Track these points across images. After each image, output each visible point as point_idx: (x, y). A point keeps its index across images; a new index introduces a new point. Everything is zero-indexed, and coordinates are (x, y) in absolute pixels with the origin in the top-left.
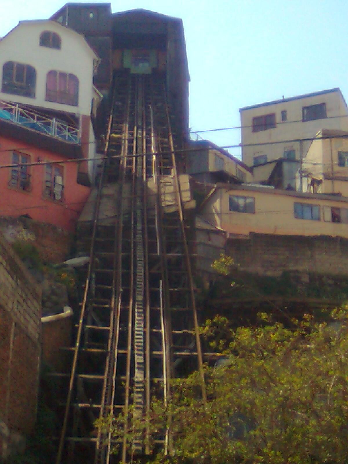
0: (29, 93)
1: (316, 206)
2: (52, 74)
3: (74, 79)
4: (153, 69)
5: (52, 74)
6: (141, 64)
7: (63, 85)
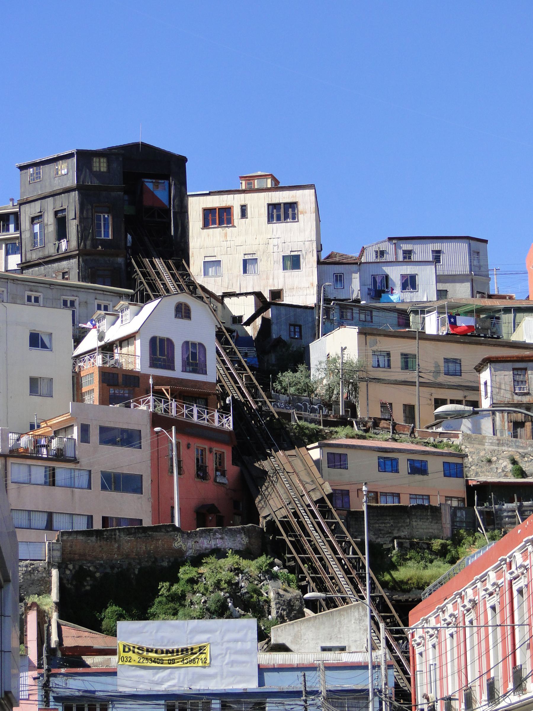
0: (171, 367)
1: (395, 459)
3: (201, 345)
5: (186, 344)
7: (195, 358)
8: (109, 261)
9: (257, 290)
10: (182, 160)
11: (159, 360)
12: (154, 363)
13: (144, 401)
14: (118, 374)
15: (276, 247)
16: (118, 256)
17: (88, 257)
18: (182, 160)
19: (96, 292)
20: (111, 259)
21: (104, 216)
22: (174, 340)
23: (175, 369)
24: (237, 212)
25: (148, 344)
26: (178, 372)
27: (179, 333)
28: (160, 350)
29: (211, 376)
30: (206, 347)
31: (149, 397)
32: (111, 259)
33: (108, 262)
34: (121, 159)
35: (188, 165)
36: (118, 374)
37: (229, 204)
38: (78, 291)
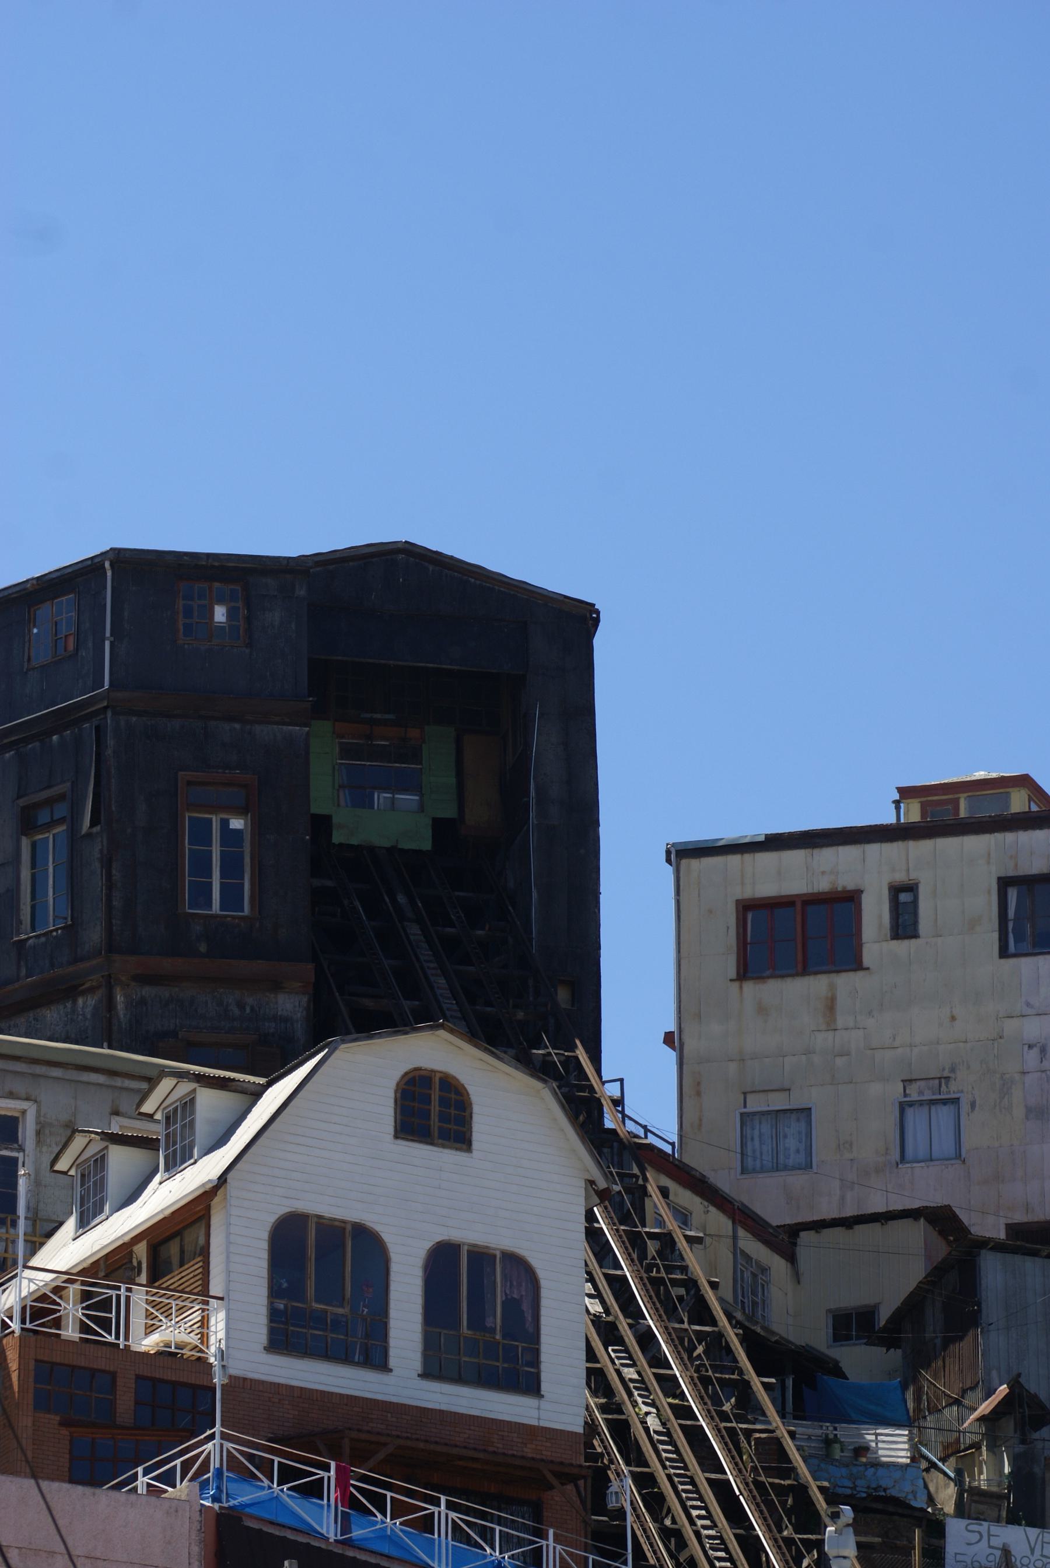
0: (374, 1356)
2: (443, 1261)
3: (518, 1266)
4: (440, 826)
6: (381, 798)
7: (481, 1305)
8: (241, 1006)
9: (935, 1199)
10: (577, 621)
11: (319, 1319)
12: (286, 1334)
13: (186, 1466)
14: (113, 1375)
15: (1035, 1051)
16: (277, 986)
17: (148, 991)
18: (577, 621)
19: (119, 1082)
20: (250, 1001)
21: (225, 823)
22: (388, 1237)
23: (392, 1362)
24: (875, 912)
25: (265, 1245)
26: (403, 1379)
27: (413, 1205)
28: (322, 1274)
29: (561, 1403)
30: (541, 1274)
31: (209, 1446)
32: (250, 1001)
33: (236, 1011)
34: (301, 592)
35: (606, 647)
36: (113, 1375)
37: (846, 882)
38: (35, 1076)
